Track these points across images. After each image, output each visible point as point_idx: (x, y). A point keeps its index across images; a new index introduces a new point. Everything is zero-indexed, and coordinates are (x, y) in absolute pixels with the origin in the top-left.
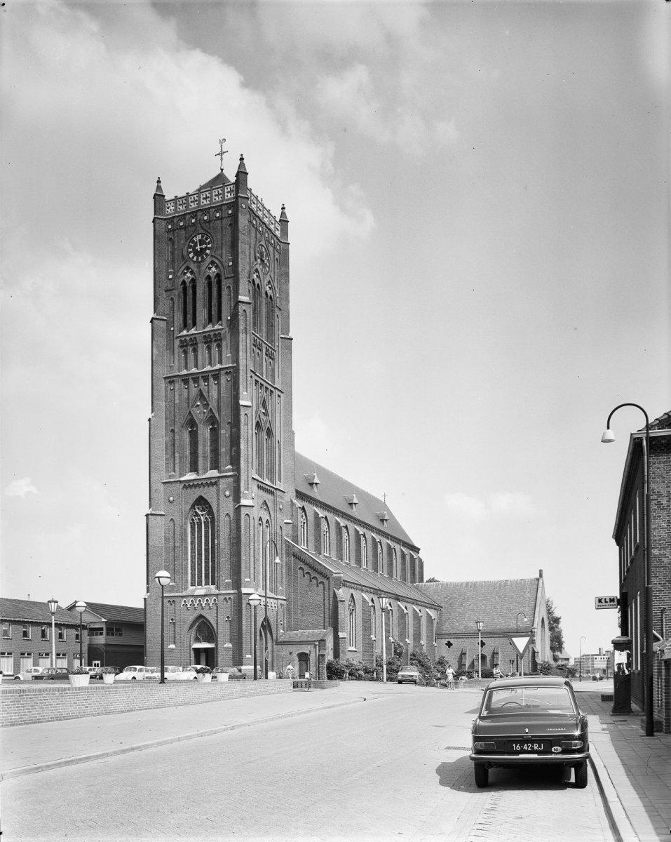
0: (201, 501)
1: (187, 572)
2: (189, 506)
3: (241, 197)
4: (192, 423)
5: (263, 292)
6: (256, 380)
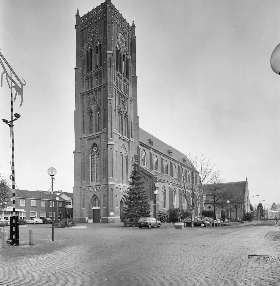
0: (95, 145)
1: (90, 176)
2: (90, 148)
3: (107, 6)
4: (91, 112)
5: (122, 55)
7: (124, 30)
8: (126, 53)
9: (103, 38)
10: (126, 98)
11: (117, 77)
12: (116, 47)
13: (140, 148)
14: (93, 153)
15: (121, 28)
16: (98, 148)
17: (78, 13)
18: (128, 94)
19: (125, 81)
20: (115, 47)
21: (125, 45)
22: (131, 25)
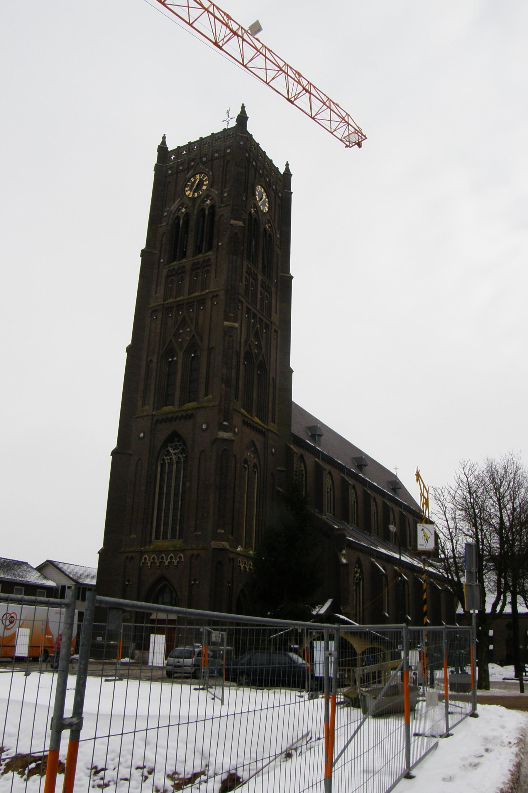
5: (262, 230)
6: (247, 307)
7: (268, 180)
8: (270, 225)
9: (222, 193)
10: (266, 323)
11: (248, 277)
12: (250, 213)
13: (295, 450)
14: (168, 457)
15: (261, 176)
16: (185, 444)
17: (164, 142)
18: (270, 316)
19: (264, 286)
20: (248, 212)
21: (267, 210)
22: (282, 171)
